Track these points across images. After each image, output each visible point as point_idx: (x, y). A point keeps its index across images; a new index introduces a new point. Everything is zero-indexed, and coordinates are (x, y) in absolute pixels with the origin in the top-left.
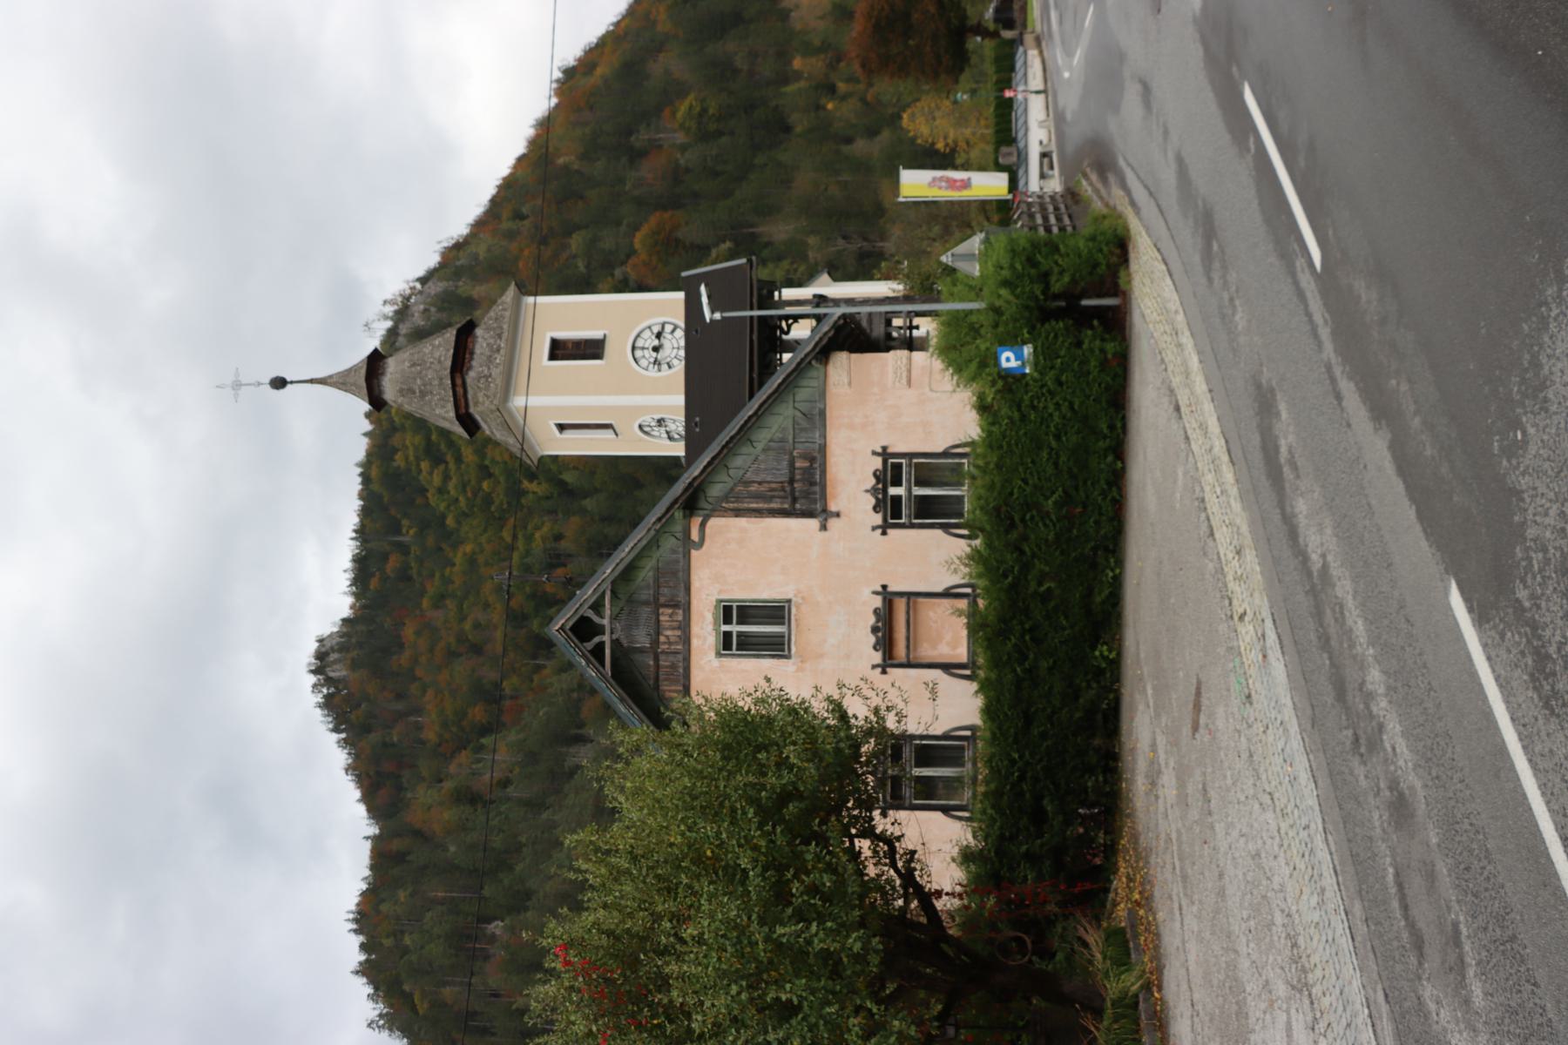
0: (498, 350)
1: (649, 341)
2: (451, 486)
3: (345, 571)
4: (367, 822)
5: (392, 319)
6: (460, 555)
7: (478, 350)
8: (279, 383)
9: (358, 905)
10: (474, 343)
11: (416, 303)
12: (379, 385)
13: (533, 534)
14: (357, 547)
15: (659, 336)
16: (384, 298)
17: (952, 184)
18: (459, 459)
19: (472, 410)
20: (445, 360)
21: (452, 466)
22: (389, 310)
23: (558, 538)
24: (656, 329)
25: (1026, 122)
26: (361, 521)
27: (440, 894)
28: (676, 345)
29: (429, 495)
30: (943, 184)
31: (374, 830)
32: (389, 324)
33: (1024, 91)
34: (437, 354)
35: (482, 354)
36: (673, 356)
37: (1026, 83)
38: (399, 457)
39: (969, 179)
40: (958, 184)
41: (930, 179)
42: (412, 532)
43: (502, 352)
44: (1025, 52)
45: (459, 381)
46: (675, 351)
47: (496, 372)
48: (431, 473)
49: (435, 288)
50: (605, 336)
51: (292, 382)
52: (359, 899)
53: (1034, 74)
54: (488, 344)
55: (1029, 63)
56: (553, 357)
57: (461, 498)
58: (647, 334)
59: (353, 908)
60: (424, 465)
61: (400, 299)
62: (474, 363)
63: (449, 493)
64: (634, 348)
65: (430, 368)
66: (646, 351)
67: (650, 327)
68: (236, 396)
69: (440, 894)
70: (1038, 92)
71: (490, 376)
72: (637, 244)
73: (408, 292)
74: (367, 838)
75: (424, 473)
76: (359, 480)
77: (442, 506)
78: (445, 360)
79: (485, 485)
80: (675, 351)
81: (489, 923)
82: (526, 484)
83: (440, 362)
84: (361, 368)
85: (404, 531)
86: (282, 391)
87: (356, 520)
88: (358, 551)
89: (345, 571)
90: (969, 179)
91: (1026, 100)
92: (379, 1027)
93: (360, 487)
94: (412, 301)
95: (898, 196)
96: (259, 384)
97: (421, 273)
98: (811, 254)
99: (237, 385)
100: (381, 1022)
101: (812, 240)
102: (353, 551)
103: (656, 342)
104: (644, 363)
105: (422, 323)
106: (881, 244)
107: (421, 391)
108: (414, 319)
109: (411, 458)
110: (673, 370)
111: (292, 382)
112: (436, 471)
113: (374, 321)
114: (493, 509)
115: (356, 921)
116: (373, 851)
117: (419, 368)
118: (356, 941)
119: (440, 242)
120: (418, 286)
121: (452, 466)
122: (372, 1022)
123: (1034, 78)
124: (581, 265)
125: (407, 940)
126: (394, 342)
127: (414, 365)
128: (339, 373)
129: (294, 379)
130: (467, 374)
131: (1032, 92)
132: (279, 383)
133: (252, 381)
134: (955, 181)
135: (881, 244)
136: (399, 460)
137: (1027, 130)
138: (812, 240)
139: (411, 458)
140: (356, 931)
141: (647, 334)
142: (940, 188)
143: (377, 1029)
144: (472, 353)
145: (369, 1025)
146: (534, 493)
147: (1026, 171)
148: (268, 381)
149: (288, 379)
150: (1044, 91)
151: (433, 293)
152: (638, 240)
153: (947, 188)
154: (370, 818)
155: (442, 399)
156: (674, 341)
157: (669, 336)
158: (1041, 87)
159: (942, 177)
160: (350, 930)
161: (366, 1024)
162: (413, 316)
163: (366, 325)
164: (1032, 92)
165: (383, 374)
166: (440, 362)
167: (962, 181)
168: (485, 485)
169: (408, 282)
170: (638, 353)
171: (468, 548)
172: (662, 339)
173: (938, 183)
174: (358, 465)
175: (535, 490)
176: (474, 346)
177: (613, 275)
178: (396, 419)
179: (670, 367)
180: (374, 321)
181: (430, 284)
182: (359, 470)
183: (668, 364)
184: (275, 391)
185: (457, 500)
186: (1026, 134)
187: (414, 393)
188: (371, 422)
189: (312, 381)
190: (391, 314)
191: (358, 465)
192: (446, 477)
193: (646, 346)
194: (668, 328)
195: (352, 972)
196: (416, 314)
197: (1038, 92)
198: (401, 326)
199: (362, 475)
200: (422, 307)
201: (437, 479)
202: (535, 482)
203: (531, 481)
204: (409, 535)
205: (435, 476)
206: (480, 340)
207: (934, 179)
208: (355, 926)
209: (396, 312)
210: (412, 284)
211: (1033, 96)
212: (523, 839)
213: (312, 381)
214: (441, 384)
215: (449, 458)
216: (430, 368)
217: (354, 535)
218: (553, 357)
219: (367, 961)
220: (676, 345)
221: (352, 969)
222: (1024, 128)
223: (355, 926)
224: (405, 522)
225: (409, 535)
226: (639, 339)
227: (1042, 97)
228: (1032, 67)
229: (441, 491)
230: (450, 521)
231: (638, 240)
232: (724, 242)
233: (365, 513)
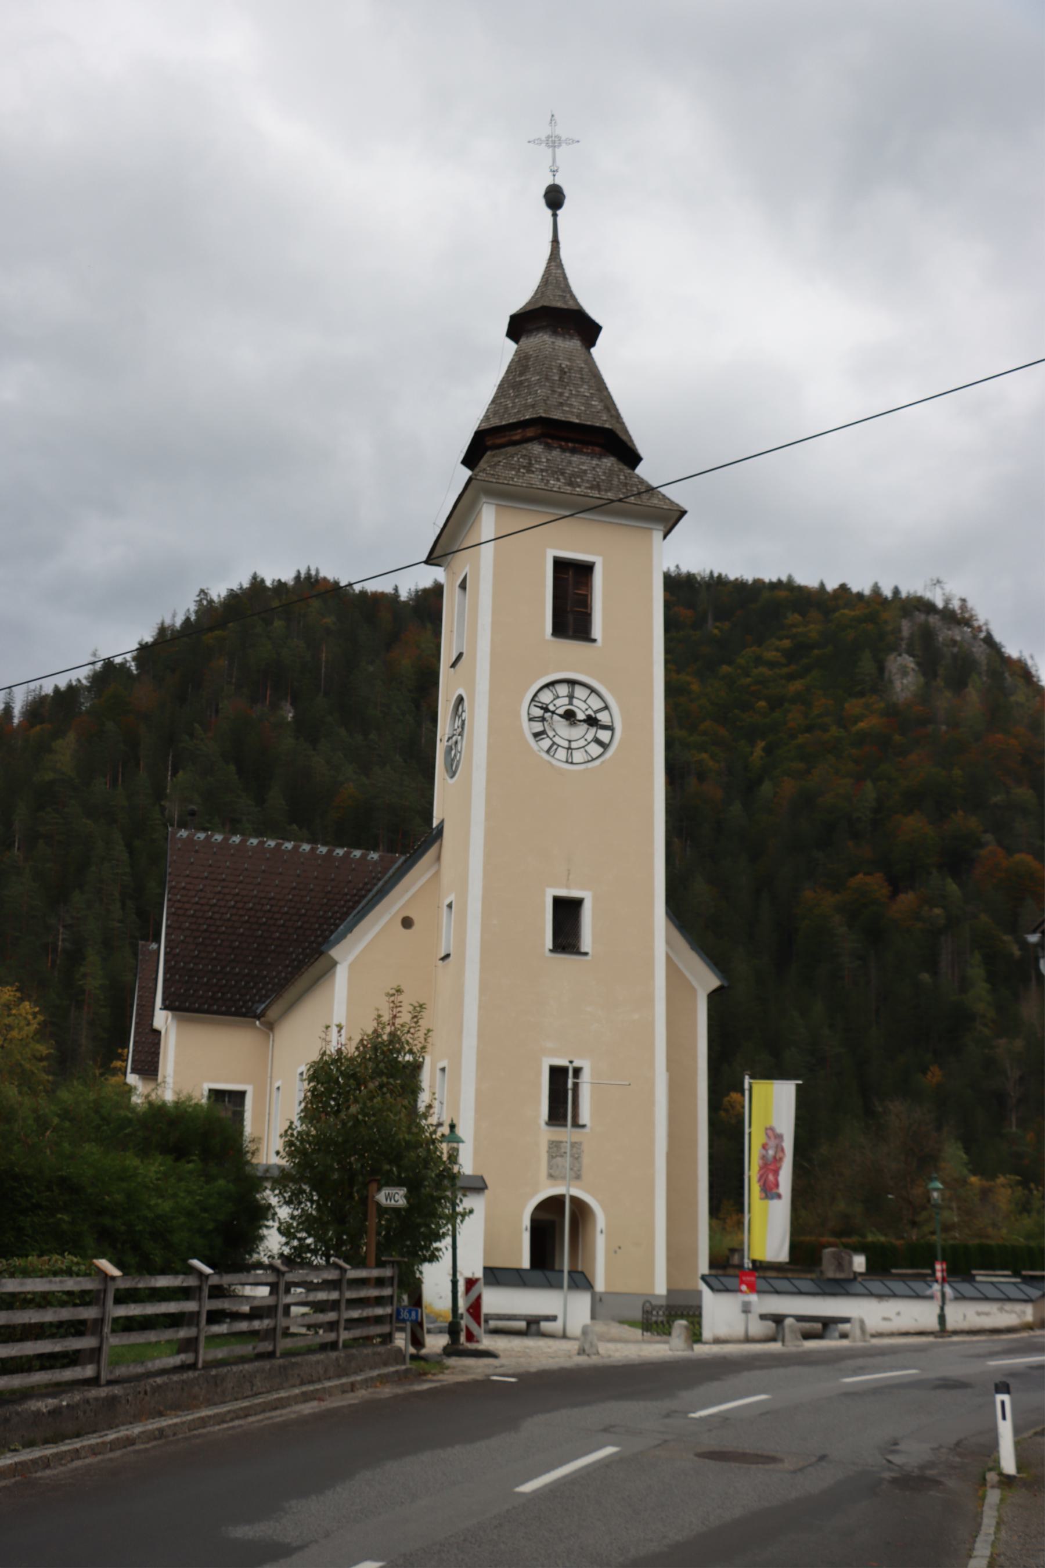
0: (571, 484)
1: (584, 706)
2: (764, 670)
3: (677, 567)
4: (413, 589)
5: (946, 607)
6: (688, 678)
7: (575, 459)
8: (554, 198)
9: (325, 579)
10: (592, 455)
11: (963, 633)
12: (538, 329)
13: (706, 752)
14: (703, 578)
15: (592, 721)
16: (968, 599)
17: (770, 1167)
18: (791, 677)
19: (489, 453)
20: (564, 412)
21: (785, 670)
22: (956, 605)
23: (701, 777)
24: (603, 717)
25: (894, 1295)
26: (730, 582)
27: (324, 655)
28: (574, 745)
29: (754, 648)
30: (771, 1152)
31: (404, 596)
32: (940, 604)
33: (943, 1295)
34: (574, 401)
35: (570, 463)
36: (557, 740)
37: (956, 1299)
38: (797, 618)
39: (779, 1196)
40: (771, 1177)
41: (779, 1131)
42: (716, 631)
43: (568, 489)
44: (1028, 1300)
45: (530, 432)
46: (566, 744)
47: (535, 479)
48: (777, 650)
49: (979, 651)
50: (594, 641)
51: (555, 215)
52: (332, 580)
53: (987, 1314)
54: (585, 472)
55: (1008, 1306)
56: (561, 565)
57: (749, 680)
58: (595, 703)
59: (322, 575)
60: (786, 643)
61: (967, 615)
62: (556, 453)
63: (756, 667)
64: (572, 683)
65: (554, 391)
66: (566, 701)
67: (606, 708)
68: (537, 142)
69: (324, 655)
70: (942, 1318)
71: (529, 471)
72: (1019, 857)
73: (976, 624)
74: (396, 589)
75: (778, 643)
76: (774, 580)
77: (741, 661)
78: (564, 412)
79: (762, 704)
80: (566, 744)
81: (291, 704)
82: (761, 744)
83: (561, 404)
84: (565, 302)
85: (718, 624)
86: (542, 202)
87: (732, 577)
88: (699, 578)
89: (677, 567)
90: (779, 1196)
91: (931, 1297)
92: (201, 601)
93: (767, 580)
94: (965, 629)
95: (752, 1077)
96: (554, 172)
97: (998, 637)
98: (1002, 1041)
99: (553, 142)
100: (205, 602)
101: (1019, 1044)
102: (699, 574)
103: (581, 716)
104: (546, 697)
105: (940, 639)
106: (1014, 1120)
107: (521, 383)
108: (945, 631)
109: (794, 630)
110: (531, 740)
111: (555, 215)
112: (779, 654)
113: (942, 589)
114: (736, 711)
115: (309, 576)
116: (383, 594)
117: (556, 378)
118: (288, 577)
119: (1032, 657)
120: (982, 635)
121: (785, 670)
122: (206, 594)
123: (979, 1314)
124: (998, 799)
125: (278, 624)
126: (919, 610)
127: (562, 372)
128: (565, 278)
129: (559, 219)
130: (540, 443)
131: (942, 1309)
132: (554, 198)
133: (558, 163)
134: (776, 1172)
135: (1014, 1120)
136: (794, 618)
137: (880, 1297)
138: (1019, 1044)
139: (794, 630)
140: (298, 578)
141: (595, 703)
142: (764, 1147)
143: (198, 599)
144: (573, 451)
145: (202, 591)
146: (752, 753)
147: (800, 1293)
148: (557, 182)
149: (559, 212)
150: (943, 1330)
151: (974, 650)
152: (1024, 858)
153: (763, 1158)
154: (417, 591)
155: (506, 408)
156: (582, 743)
157: (590, 736)
158: (951, 1324)
159: (783, 1150)
160: (299, 572)
161: (204, 587)
162: (949, 629)
163: (939, 582)
164: (942, 1309)
165: (555, 333)
166: (561, 404)
167: (777, 1185)
168: (762, 704)
169: (986, 624)
170: (563, 690)
171: (695, 687)
172: (585, 726)
173: (772, 1143)
174: (790, 578)
175: (755, 754)
176: (587, 454)
177: (985, 831)
178: (837, 614)
179: (536, 735)
180: (942, 589)
181: (984, 646)
182: (784, 579)
183: (543, 732)
184: (543, 192)
185: (748, 676)
186: (871, 1295)
187: (521, 375)
188: (835, 591)
189: (555, 242)
190: (951, 606)
191: (790, 578)
192: (772, 665)
193: (575, 702)
194: (604, 736)
195: (255, 574)
196: (950, 633)
197: (942, 1318)
198: (937, 617)
199: (780, 582)
200: (958, 638)
201: (771, 655)
202: (763, 754)
203: (764, 749)
204: (714, 628)
205: (774, 653)
206: (595, 462)
207: (779, 1137)
208: (303, 576)
209: (953, 613)
210: (984, 628)
211: (937, 1311)
212: (373, 736)
213: (555, 242)
214: (527, 407)
215: (793, 667)
216: (554, 391)
217: (716, 575)
218: (561, 565)
219: (266, 588)
220: (574, 745)
221: (257, 573)
222: (884, 1290)
223: (303, 576)
224: (727, 625)
225: (714, 628)
226: (587, 692)
227: (933, 1324)
228: (1001, 1310)
229: (758, 661)
230: (725, 669)
231: (1024, 858)
232: (1020, 949)
233: (740, 586)
